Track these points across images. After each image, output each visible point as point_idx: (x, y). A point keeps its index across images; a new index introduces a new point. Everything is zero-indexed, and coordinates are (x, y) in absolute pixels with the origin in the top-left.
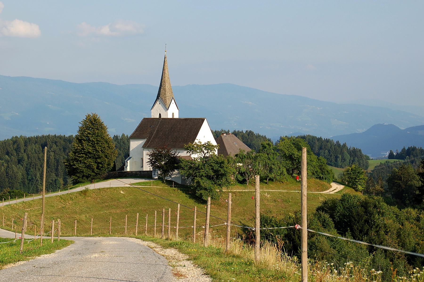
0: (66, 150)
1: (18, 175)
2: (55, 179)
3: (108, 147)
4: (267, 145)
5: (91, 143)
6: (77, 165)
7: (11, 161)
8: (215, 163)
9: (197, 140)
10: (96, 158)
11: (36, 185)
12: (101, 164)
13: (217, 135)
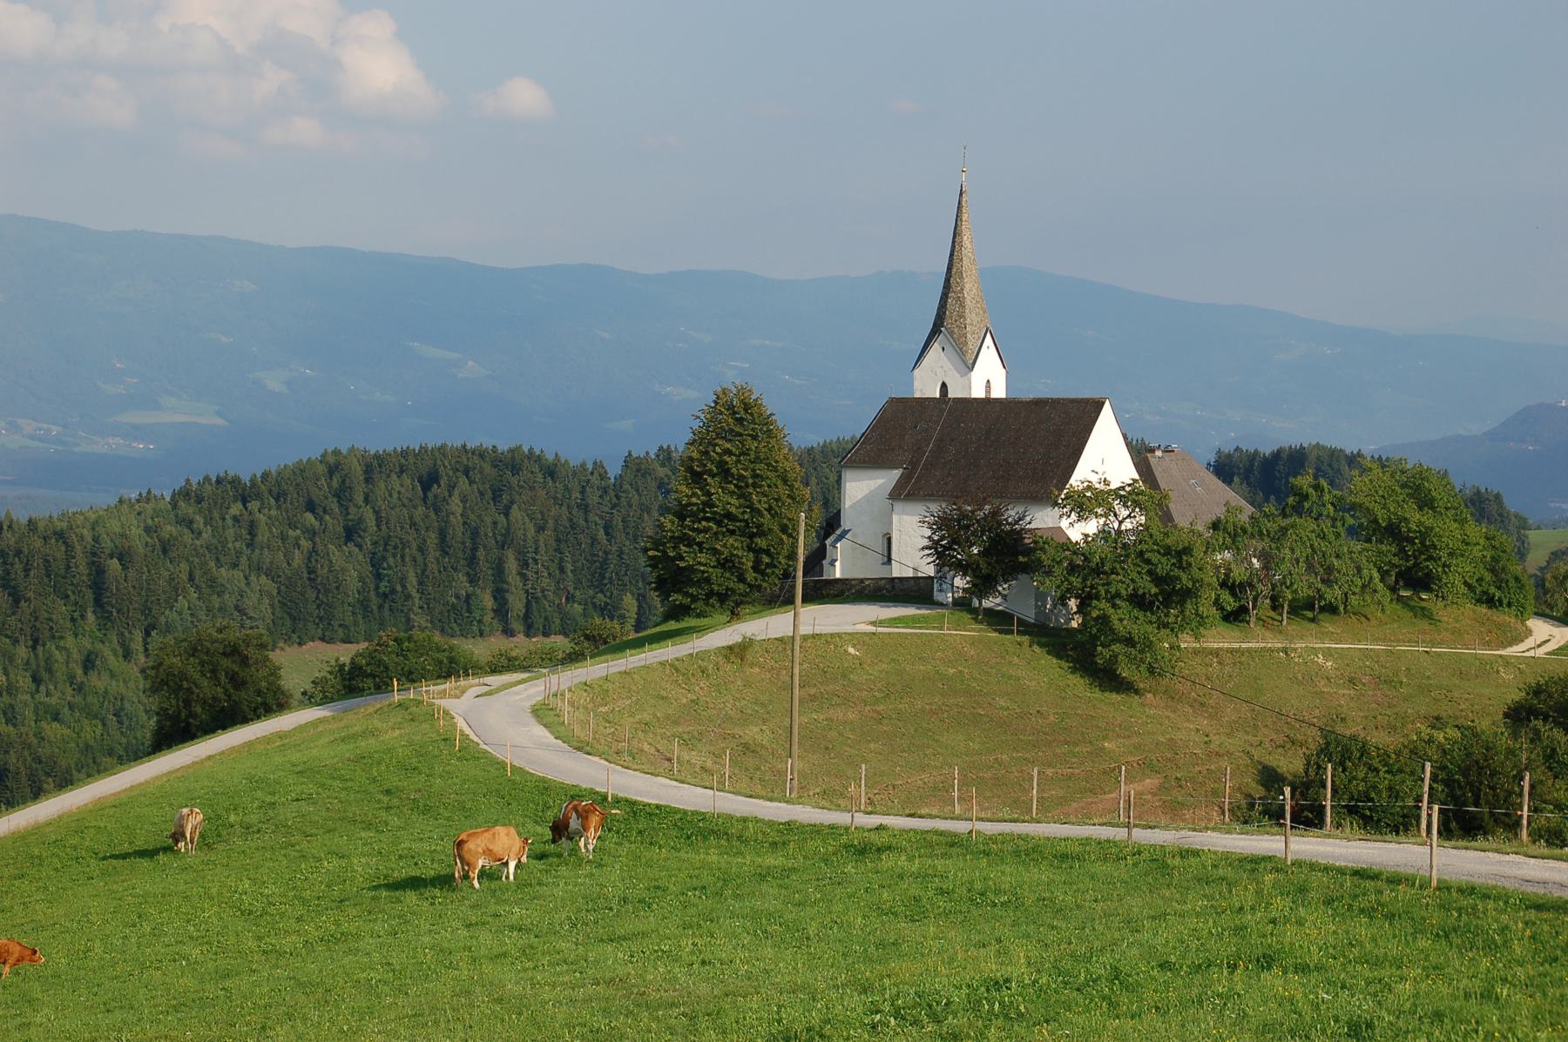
0: (501, 496)
1: (346, 580)
2: (466, 592)
3: (789, 496)
4: (1311, 490)
5: (736, 486)
6: (690, 558)
7: (324, 532)
8: (1159, 552)
9: (1097, 473)
10: (751, 533)
11: (406, 611)
12: (767, 555)
13: (1140, 453)
